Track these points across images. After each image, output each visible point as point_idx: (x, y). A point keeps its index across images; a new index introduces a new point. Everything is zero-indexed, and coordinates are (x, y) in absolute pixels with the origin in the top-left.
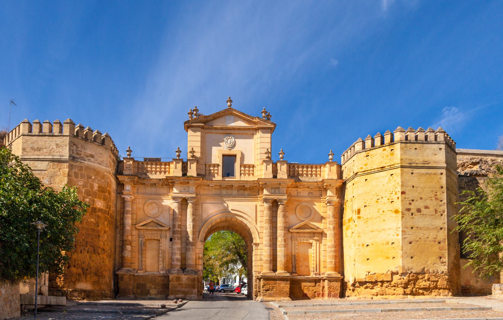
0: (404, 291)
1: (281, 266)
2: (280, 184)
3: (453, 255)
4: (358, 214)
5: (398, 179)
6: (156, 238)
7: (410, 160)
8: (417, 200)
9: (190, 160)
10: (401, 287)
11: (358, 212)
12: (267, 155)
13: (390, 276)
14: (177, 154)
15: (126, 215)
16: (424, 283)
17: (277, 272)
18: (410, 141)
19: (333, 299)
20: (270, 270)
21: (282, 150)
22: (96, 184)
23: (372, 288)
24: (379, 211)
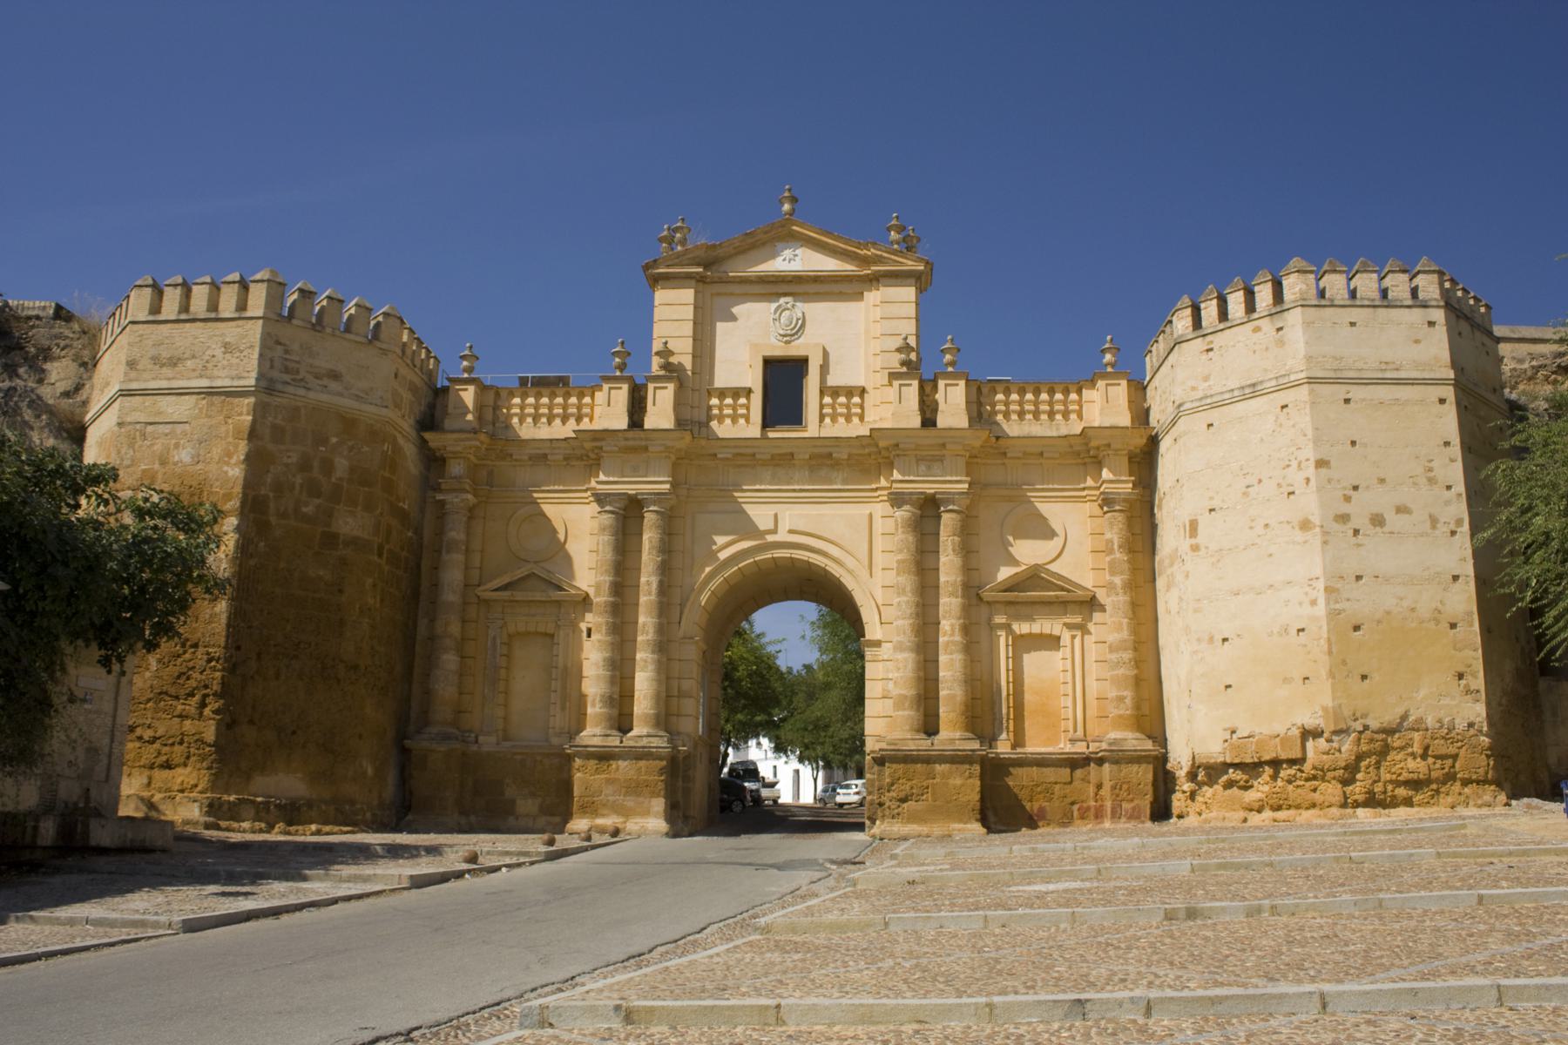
0: (1344, 793)
1: (952, 715)
2: (944, 445)
4: (1191, 537)
5: (1303, 420)
6: (541, 629)
7: (1335, 358)
9: (657, 378)
10: (1334, 778)
11: (1190, 530)
13: (1299, 741)
15: (445, 557)
16: (1412, 764)
17: (937, 737)
18: (1332, 300)
19: (1127, 825)
20: (918, 731)
23: (1246, 788)
24: (1253, 524)
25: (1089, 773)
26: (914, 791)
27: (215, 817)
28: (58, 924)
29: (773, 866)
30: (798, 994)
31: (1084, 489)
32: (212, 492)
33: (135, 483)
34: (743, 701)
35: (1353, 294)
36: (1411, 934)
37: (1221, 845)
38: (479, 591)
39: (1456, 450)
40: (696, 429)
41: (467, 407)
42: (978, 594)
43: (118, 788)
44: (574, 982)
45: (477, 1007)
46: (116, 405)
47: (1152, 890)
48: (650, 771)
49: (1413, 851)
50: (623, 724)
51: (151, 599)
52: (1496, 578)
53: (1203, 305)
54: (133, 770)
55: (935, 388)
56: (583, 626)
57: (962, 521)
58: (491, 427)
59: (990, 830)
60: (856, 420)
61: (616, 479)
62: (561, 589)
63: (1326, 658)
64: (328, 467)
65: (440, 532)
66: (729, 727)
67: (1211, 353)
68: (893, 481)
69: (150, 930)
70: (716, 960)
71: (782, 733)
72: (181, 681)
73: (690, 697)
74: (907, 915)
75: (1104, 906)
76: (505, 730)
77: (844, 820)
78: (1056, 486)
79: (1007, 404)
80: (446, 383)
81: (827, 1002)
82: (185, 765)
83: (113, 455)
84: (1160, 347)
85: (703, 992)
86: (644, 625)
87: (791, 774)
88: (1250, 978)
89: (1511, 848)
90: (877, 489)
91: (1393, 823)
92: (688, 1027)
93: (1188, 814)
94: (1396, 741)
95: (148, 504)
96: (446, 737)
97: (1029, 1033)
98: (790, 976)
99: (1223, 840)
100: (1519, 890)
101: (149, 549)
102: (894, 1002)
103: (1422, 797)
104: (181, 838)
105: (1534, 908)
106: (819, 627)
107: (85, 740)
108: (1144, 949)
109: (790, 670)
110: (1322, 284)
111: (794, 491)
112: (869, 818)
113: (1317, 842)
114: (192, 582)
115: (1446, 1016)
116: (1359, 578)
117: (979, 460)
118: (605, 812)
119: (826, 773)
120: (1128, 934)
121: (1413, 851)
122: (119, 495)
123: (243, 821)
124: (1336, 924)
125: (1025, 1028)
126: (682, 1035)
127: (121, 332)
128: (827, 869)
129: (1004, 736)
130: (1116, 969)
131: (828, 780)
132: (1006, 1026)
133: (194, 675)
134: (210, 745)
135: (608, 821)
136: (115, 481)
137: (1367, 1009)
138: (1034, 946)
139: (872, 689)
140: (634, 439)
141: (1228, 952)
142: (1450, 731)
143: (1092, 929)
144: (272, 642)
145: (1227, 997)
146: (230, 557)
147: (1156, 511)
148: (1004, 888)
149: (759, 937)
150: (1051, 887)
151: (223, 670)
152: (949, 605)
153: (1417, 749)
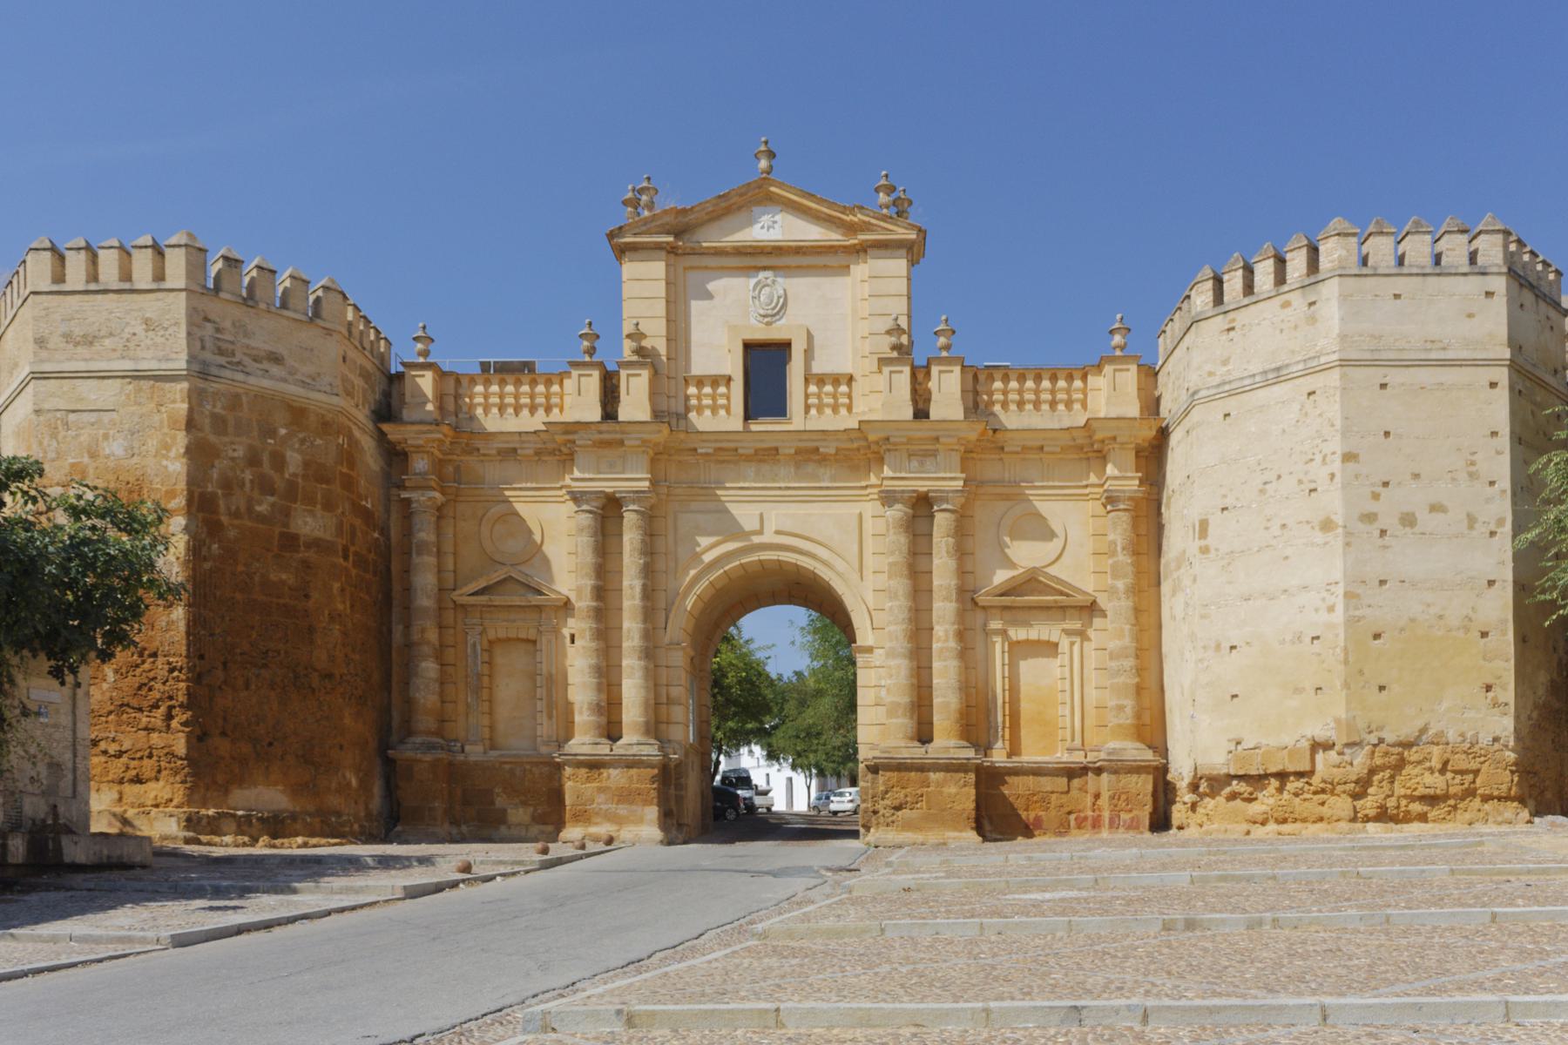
0: (1355, 807)
2: (937, 439)
3: (1543, 678)
4: (1200, 538)
5: (1332, 409)
6: (522, 635)
7: (1372, 336)
8: (1400, 483)
9: (630, 364)
10: (1344, 792)
12: (893, 339)
13: (1308, 753)
14: (586, 343)
15: (416, 559)
16: (1428, 779)
17: (932, 745)
18: (1375, 269)
19: (1125, 836)
20: (912, 739)
21: (947, 320)
22: (296, 455)
23: (1250, 800)
25: (1087, 783)
26: (908, 799)
27: (194, 832)
28: (42, 941)
29: (768, 873)
30: (796, 998)
31: (1087, 486)
32: (153, 489)
33: (64, 478)
34: (733, 709)
35: (1401, 261)
36: (1420, 950)
37: (1222, 857)
38: (455, 595)
39: (1504, 441)
40: (674, 422)
41: (425, 395)
42: (973, 599)
43: (87, 803)
44: (575, 987)
45: (479, 1014)
46: (30, 389)
47: (1150, 900)
48: (643, 780)
49: (1425, 867)
50: (612, 732)
51: (99, 606)
52: (1537, 584)
53: (1226, 277)
54: (102, 785)
55: (928, 374)
56: (566, 632)
57: (957, 520)
58: (454, 418)
59: (985, 839)
60: (843, 411)
61: (591, 476)
62: (541, 593)
63: (1341, 667)
64: (279, 462)
65: (408, 532)
66: (720, 735)
67: (1232, 333)
68: (883, 479)
69: (137, 946)
70: (715, 965)
71: (773, 741)
72: (143, 693)
73: (680, 704)
74: (903, 921)
75: (1101, 915)
76: (491, 739)
77: (839, 828)
78: (1057, 484)
79: (1005, 393)
80: (401, 369)
81: (825, 1006)
82: (157, 779)
83: (34, 446)
84: (1175, 328)
85: (703, 996)
86: (629, 631)
87: (784, 783)
88: (1249, 989)
89: (1531, 866)
90: (866, 487)
91: (1405, 838)
92: (689, 1030)
93: (1188, 825)
94: (1412, 755)
95: (82, 502)
96: (431, 747)
97: (1025, 1037)
98: (788, 980)
99: (1225, 853)
100: (1536, 908)
101: (90, 552)
102: (891, 1006)
103: (1439, 812)
104: (160, 853)
105: (1550, 926)
106: (809, 633)
107: (45, 754)
108: (1141, 958)
109: (780, 678)
110: (1365, 249)
111: (780, 488)
112: (863, 826)
113: (1323, 856)
114: (143, 587)
115: (1451, 1030)
116: (1383, 582)
117: (974, 455)
118: (599, 820)
119: (820, 781)
120: (1125, 943)
121: (1425, 867)
122: (48, 491)
123: (225, 835)
124: (1341, 938)
125: (1022, 1032)
126: (684, 1038)
127: (22, 304)
128: (822, 876)
129: (999, 744)
130: (1113, 977)
131: (821, 788)
132: (1003, 1030)
133: (157, 686)
134: (181, 759)
135: (603, 829)
136: (41, 476)
137: (1369, 1022)
138: (1030, 954)
139: (864, 697)
140: (608, 432)
141: (1227, 964)
142: (1472, 745)
143: (1089, 937)
144: (238, 651)
145: (1225, 1007)
146: (182, 559)
147: (1163, 510)
148: (999, 896)
149: (756, 943)
150: (1048, 896)
151: (188, 680)
152: (943, 611)
153: (1436, 763)
